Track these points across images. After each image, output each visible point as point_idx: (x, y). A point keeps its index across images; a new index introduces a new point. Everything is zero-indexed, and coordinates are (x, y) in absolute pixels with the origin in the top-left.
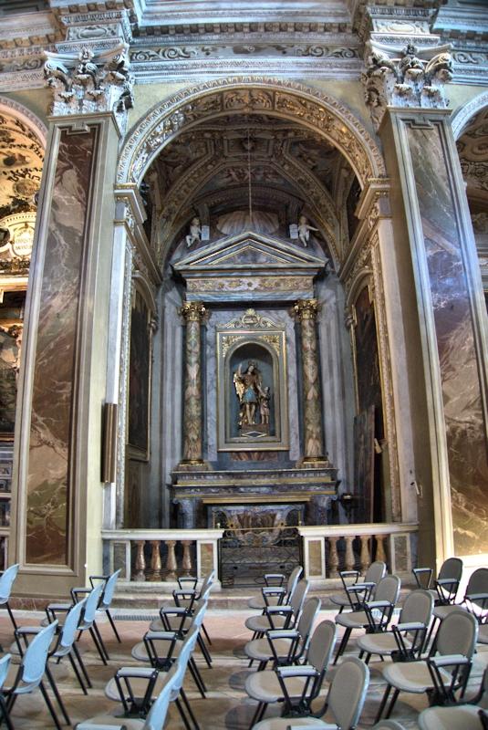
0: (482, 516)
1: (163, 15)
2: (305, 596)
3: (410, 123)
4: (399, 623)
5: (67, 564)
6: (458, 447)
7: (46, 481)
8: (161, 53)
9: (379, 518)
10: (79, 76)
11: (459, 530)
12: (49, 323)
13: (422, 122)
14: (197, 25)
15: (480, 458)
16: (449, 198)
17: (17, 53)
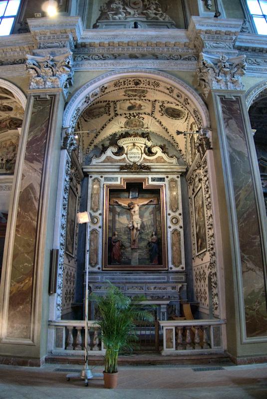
1: (247, 41)
7: (253, 291)
12: (241, 203)
14: (263, 48)
16: (37, 207)
17: (165, 50)
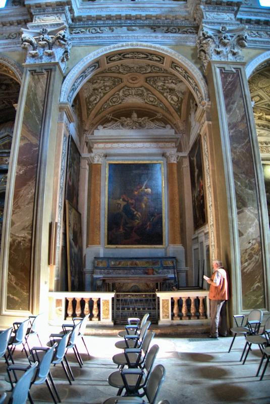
0: (23, 289)
3: (33, 72)
5: (265, 308)
6: (15, 250)
8: (88, 31)
9: (201, 288)
10: (41, 42)
11: (10, 295)
13: (41, 71)
15: (26, 257)
16: (41, 112)
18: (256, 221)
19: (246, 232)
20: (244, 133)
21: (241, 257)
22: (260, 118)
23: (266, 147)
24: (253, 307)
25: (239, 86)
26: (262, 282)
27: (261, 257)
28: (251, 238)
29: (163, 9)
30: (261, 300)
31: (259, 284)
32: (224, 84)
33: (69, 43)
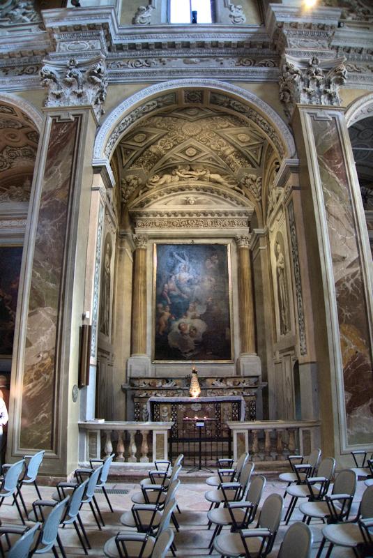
2: (251, 473)
4: (332, 494)
5: (52, 449)
18: (54, 326)
19: (36, 341)
20: (62, 203)
21: (25, 375)
22: (201, 178)
23: (204, 219)
24: (36, 445)
25: (73, 139)
26: (51, 413)
27: (52, 378)
28: (41, 349)
29: (18, 45)
30: (46, 437)
31: (46, 415)
32: (52, 137)
33: (105, 79)
